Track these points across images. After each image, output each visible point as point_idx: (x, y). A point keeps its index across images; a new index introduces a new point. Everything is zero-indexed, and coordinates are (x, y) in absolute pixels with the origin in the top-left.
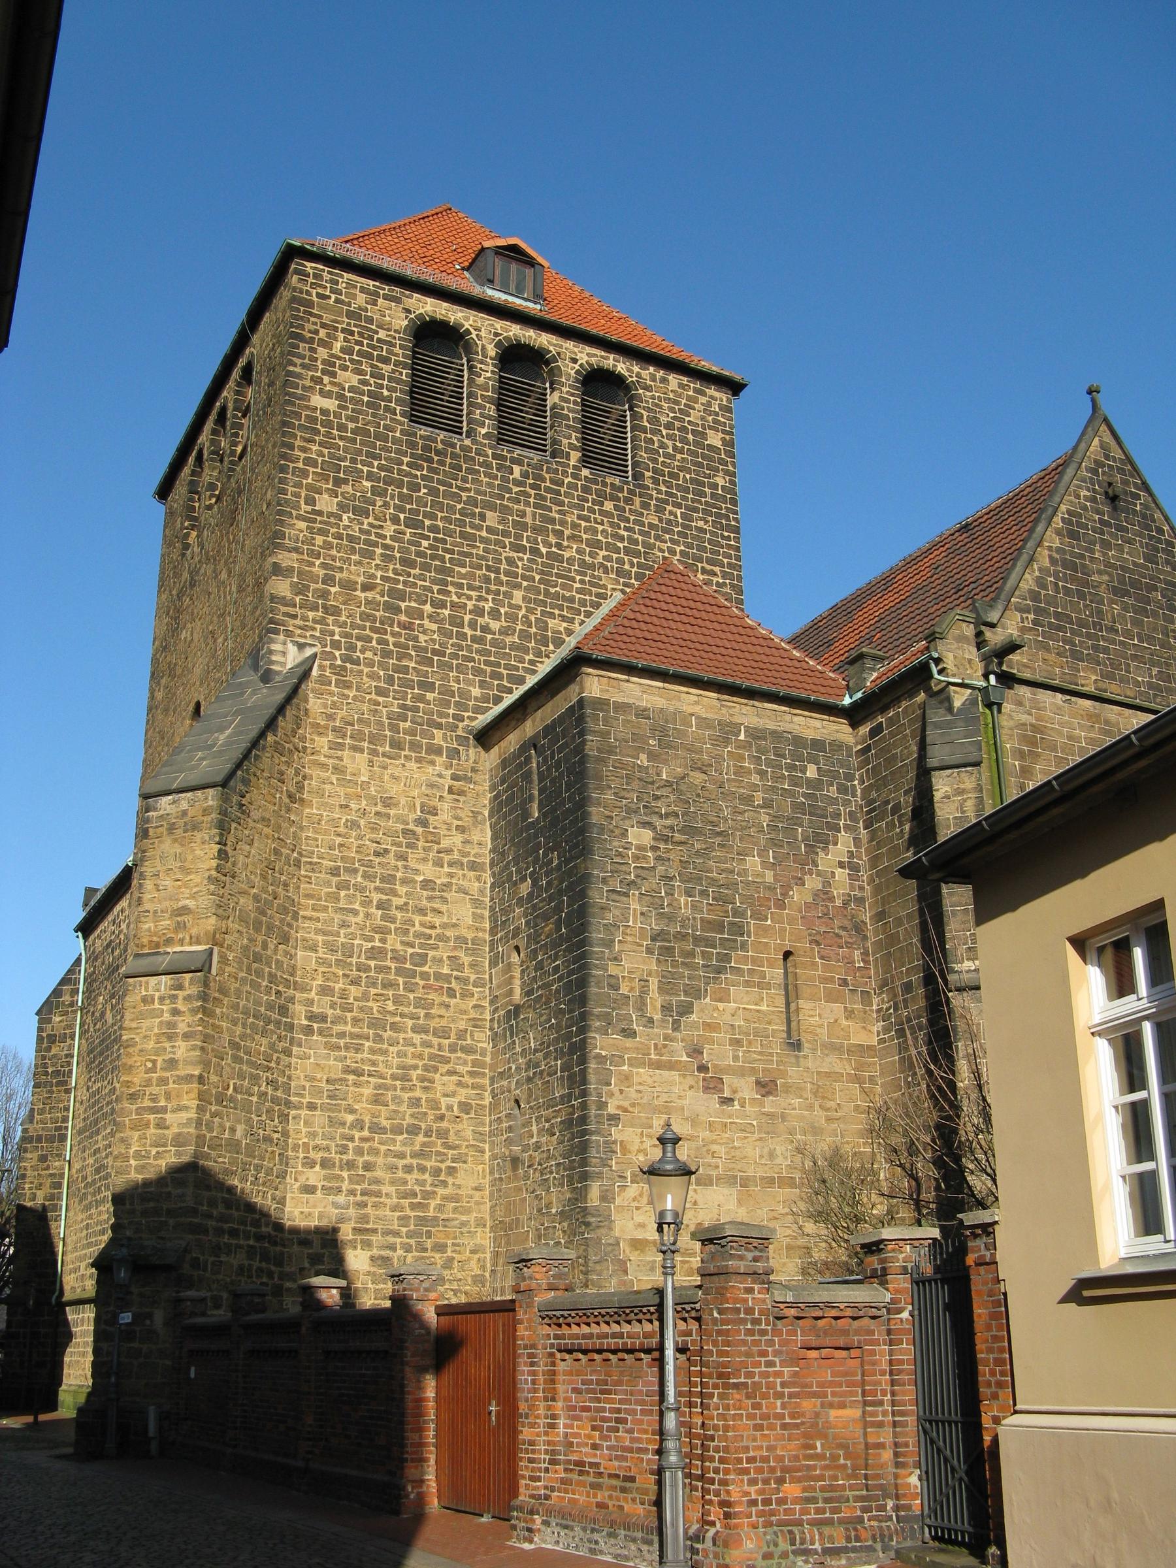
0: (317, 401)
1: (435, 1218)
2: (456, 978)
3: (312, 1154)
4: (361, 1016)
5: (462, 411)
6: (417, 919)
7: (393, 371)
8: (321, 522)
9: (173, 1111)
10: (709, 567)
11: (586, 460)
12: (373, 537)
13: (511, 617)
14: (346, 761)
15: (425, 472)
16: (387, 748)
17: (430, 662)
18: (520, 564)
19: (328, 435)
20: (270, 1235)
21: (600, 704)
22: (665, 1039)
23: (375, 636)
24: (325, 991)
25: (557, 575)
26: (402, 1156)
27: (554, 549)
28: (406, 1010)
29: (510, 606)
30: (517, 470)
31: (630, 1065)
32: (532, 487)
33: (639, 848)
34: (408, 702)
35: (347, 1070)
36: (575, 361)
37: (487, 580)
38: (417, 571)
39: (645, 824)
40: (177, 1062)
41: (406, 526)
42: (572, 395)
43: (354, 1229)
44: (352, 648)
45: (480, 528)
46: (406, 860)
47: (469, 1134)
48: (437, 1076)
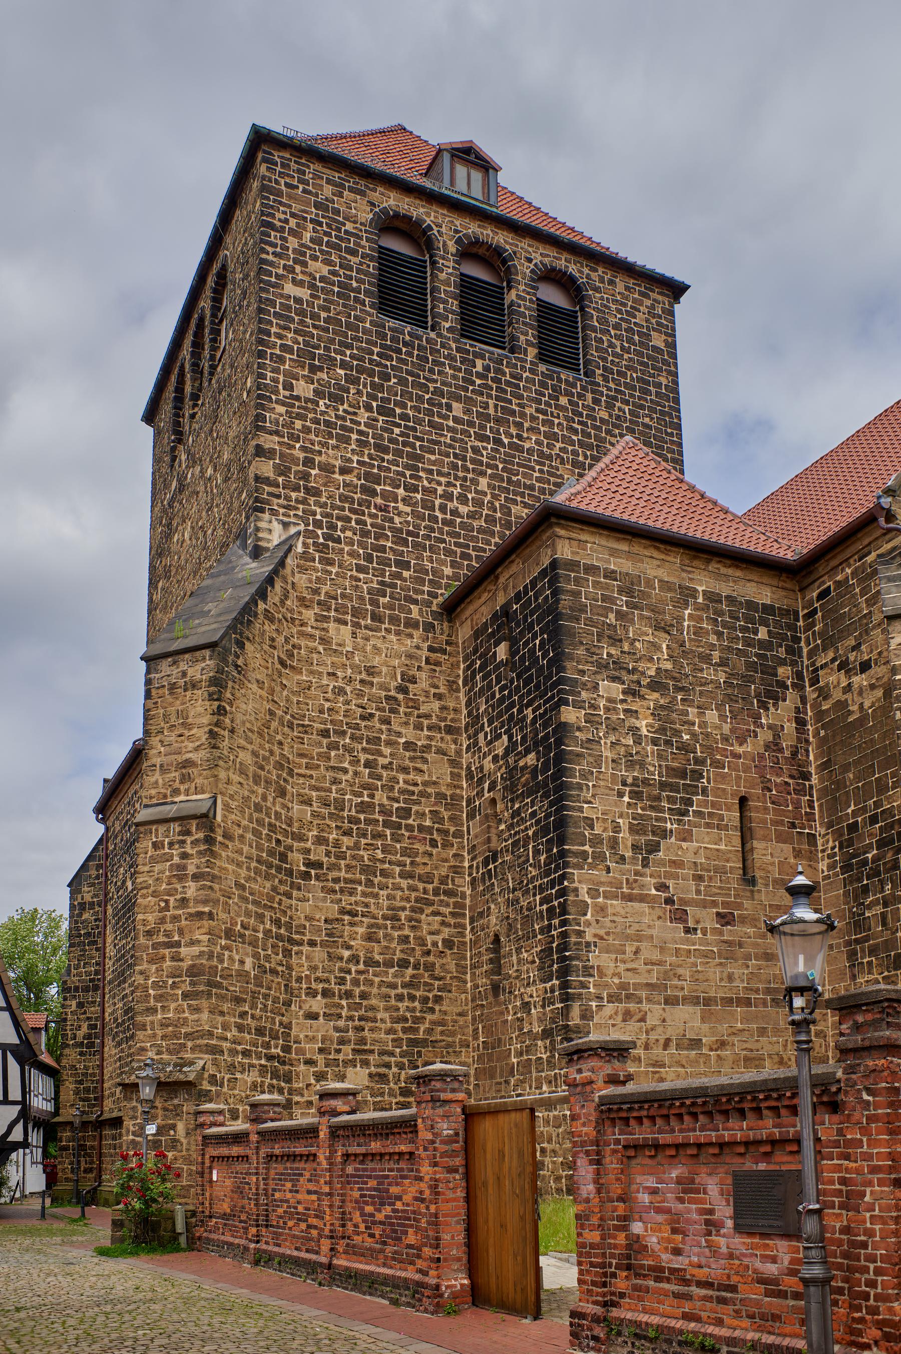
0: (289, 289)
2: (438, 830)
3: (314, 986)
4: (354, 863)
6: (401, 777)
7: (361, 264)
8: (299, 407)
11: (542, 357)
12: (348, 423)
13: (478, 503)
14: (332, 633)
17: (405, 543)
18: (484, 453)
19: (302, 322)
22: (635, 874)
23: (354, 517)
24: (320, 840)
26: (393, 986)
29: (477, 492)
30: (479, 363)
31: (605, 897)
33: (609, 700)
34: (387, 579)
35: (343, 911)
36: (530, 260)
37: (455, 467)
38: (390, 457)
39: (614, 679)
42: (528, 293)
43: (353, 1050)
44: (333, 527)
45: (446, 418)
46: (389, 723)
47: (452, 967)
48: (423, 917)
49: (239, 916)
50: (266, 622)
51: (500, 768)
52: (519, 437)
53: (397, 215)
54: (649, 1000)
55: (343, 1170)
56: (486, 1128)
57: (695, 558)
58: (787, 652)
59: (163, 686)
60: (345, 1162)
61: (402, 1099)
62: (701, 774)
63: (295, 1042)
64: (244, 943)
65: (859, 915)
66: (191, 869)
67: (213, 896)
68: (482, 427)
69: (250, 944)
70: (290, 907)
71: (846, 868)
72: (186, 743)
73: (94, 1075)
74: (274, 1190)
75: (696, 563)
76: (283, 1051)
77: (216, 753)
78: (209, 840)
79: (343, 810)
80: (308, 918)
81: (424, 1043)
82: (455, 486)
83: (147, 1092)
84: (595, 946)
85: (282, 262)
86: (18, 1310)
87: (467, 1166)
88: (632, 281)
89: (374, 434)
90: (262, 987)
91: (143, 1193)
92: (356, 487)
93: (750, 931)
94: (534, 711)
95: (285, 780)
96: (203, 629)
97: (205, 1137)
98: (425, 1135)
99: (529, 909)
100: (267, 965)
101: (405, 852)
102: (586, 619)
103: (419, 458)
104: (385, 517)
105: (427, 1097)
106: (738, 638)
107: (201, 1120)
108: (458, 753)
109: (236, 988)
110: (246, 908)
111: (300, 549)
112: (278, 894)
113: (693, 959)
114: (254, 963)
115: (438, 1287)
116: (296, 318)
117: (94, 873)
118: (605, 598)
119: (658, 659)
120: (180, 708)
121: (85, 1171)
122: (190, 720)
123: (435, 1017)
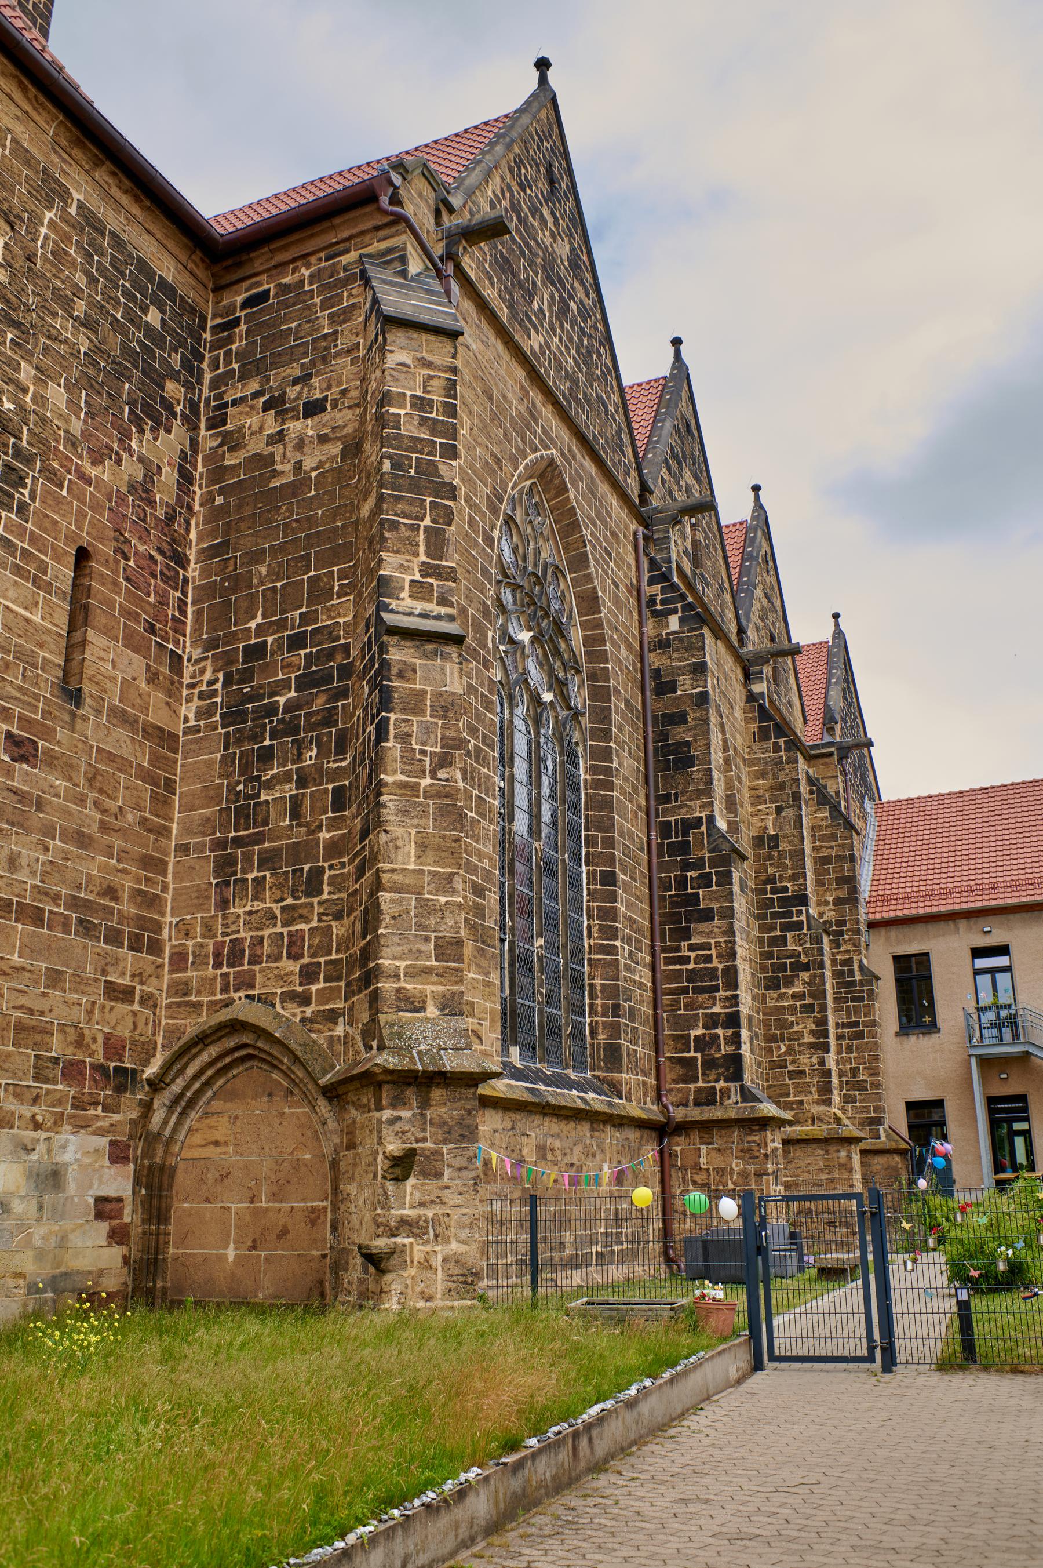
57: (78, 143)
62: (22, 479)
65: (248, 797)
71: (234, 716)
75: (76, 152)
93: (61, 784)
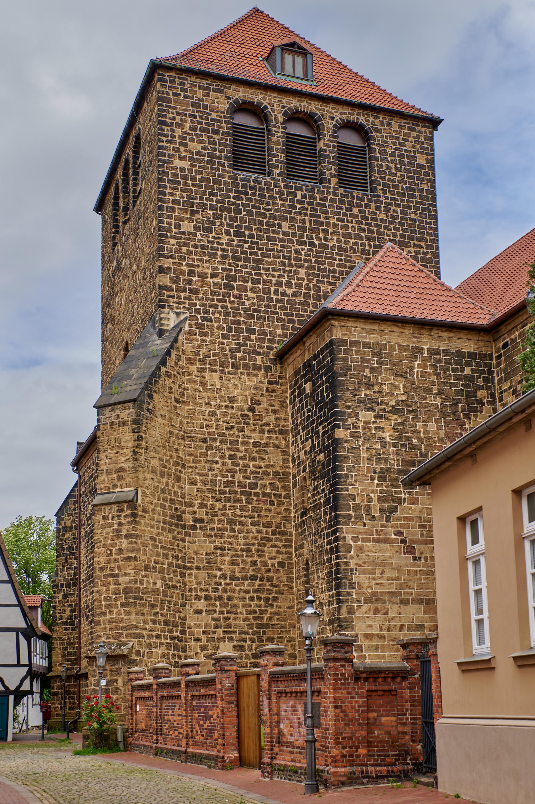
0: (177, 163)
1: (268, 624)
2: (275, 495)
3: (199, 593)
4: (223, 518)
5: (265, 159)
6: (251, 464)
7: (222, 139)
8: (184, 239)
9: (122, 576)
10: (417, 243)
11: (341, 183)
12: (215, 245)
13: (299, 286)
14: (207, 378)
15: (244, 202)
16: (230, 369)
17: (252, 317)
18: (303, 253)
19: (185, 184)
20: (178, 636)
21: (342, 342)
22: (382, 527)
23: (220, 304)
24: (202, 506)
25: (326, 258)
26: (248, 592)
27: (323, 241)
28: (247, 514)
29: (298, 279)
30: (299, 194)
31: (362, 541)
32: (308, 203)
33: (365, 422)
34: (241, 341)
35: (216, 548)
36: (332, 118)
37: (284, 264)
38: (242, 263)
39: (368, 409)
40: (123, 550)
41: (235, 236)
42: (332, 141)
43: (223, 631)
44: (207, 312)
45: (278, 233)
46: (244, 431)
47: (284, 579)
48: (266, 548)
49: (152, 556)
50: (166, 378)
51: (308, 459)
52: (326, 239)
53: (244, 102)
54: (390, 602)
55: (191, 703)
56: (244, 682)
57: (422, 329)
58: (484, 382)
59: (107, 424)
60: (192, 699)
61: (253, 661)
63: (188, 628)
64: (156, 572)
66: (124, 532)
67: (137, 547)
68: (301, 236)
69: (159, 572)
70: (185, 547)
72: (120, 458)
73: (74, 643)
74: (164, 715)
75: (423, 332)
76: (181, 633)
77: (138, 463)
78: (134, 515)
79: (216, 486)
80: (196, 553)
81: (267, 626)
82: (284, 276)
83: (101, 661)
84: (356, 570)
85: (172, 146)
86: (35, 774)
87: (238, 700)
88: (403, 121)
89: (232, 250)
90: (167, 596)
91: (99, 719)
92: (221, 285)
94: (324, 428)
95: (180, 472)
96: (129, 388)
97: (133, 687)
98: (219, 686)
99: (322, 547)
100: (171, 583)
101: (254, 510)
102: (351, 374)
103: (260, 262)
104: (240, 302)
105: (219, 668)
106: (450, 376)
107: (130, 677)
108: (287, 446)
109: (151, 599)
110: (157, 551)
111: (187, 328)
112: (177, 540)
113: (418, 576)
114: (162, 583)
115: (223, 757)
116: (182, 181)
117: (72, 506)
118: (363, 360)
119: (397, 394)
120: (116, 437)
121: (70, 709)
122: (122, 444)
123: (274, 610)
